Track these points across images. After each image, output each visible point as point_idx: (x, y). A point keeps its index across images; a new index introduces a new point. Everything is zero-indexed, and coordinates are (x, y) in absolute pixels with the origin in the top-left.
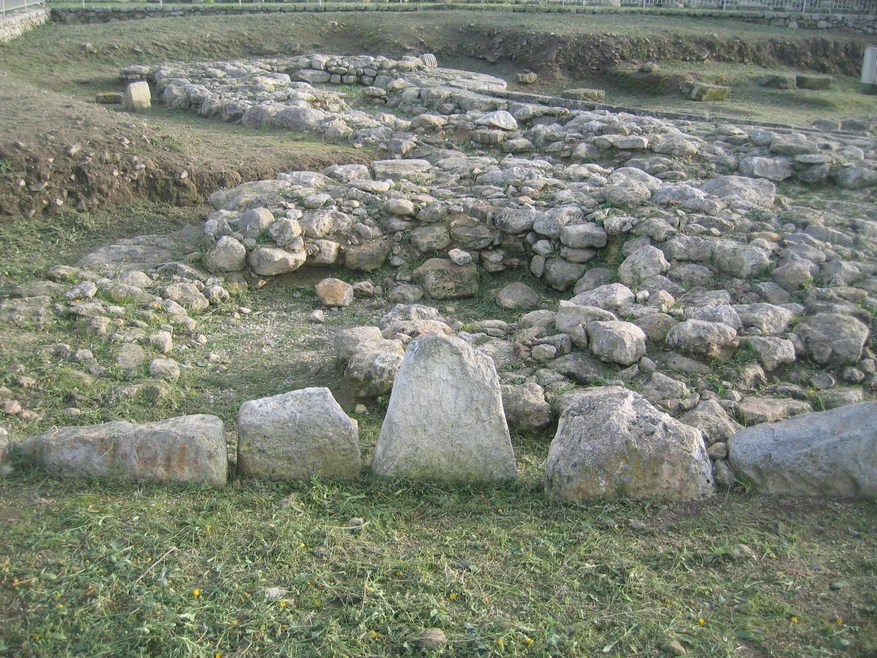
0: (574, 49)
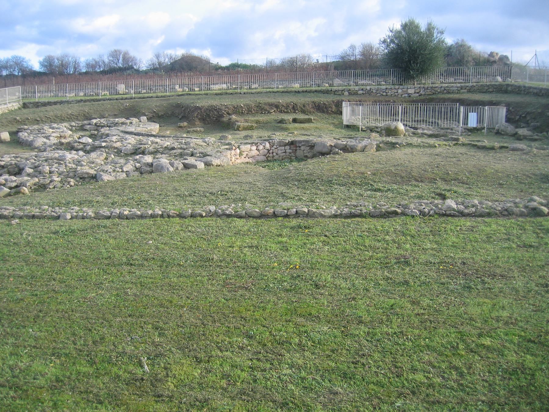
0: (205, 111)
